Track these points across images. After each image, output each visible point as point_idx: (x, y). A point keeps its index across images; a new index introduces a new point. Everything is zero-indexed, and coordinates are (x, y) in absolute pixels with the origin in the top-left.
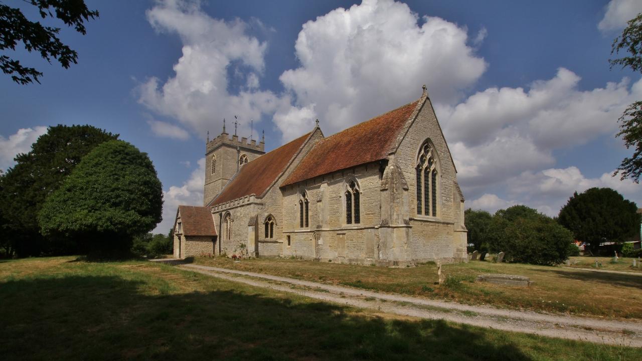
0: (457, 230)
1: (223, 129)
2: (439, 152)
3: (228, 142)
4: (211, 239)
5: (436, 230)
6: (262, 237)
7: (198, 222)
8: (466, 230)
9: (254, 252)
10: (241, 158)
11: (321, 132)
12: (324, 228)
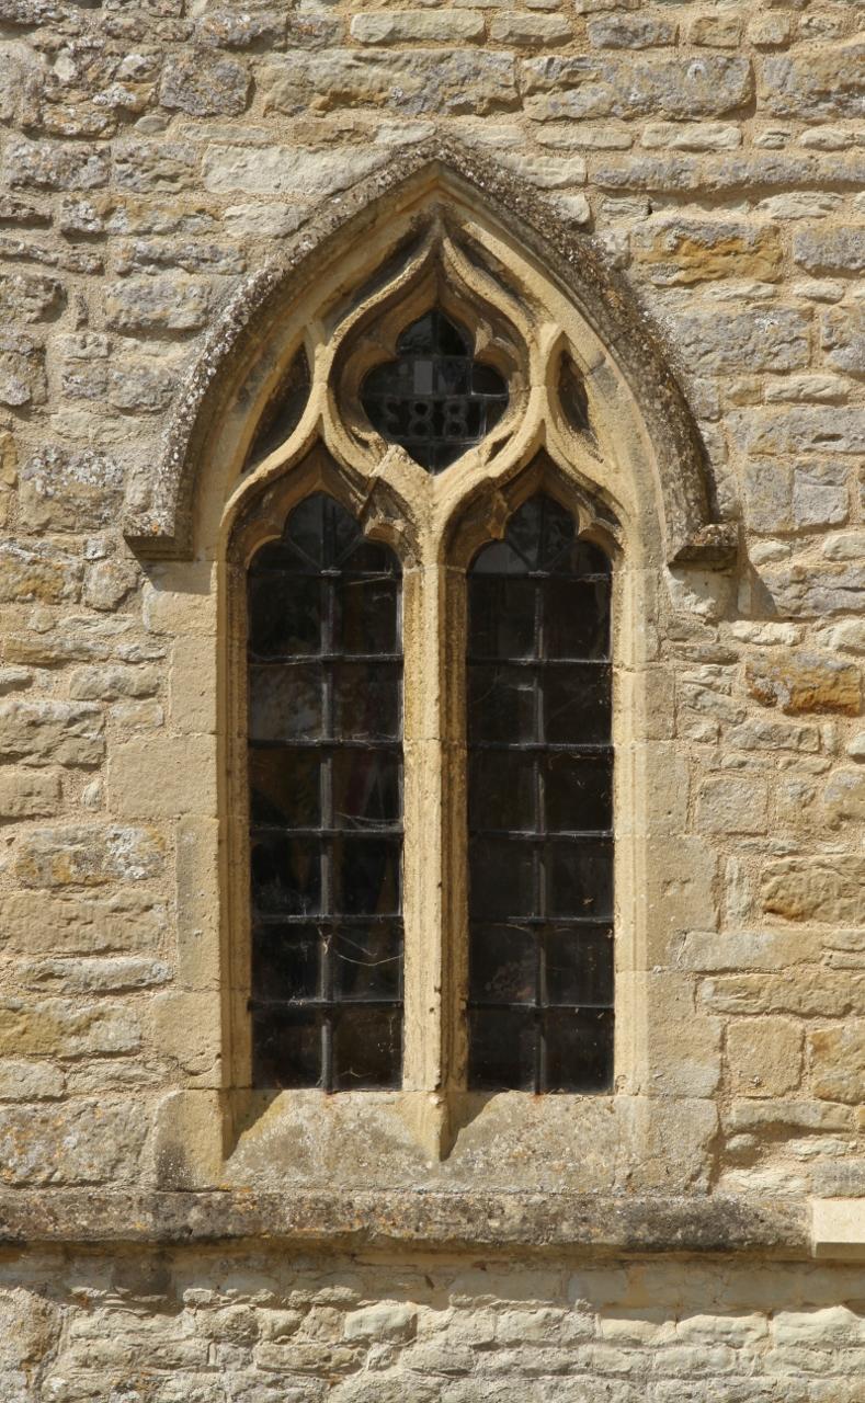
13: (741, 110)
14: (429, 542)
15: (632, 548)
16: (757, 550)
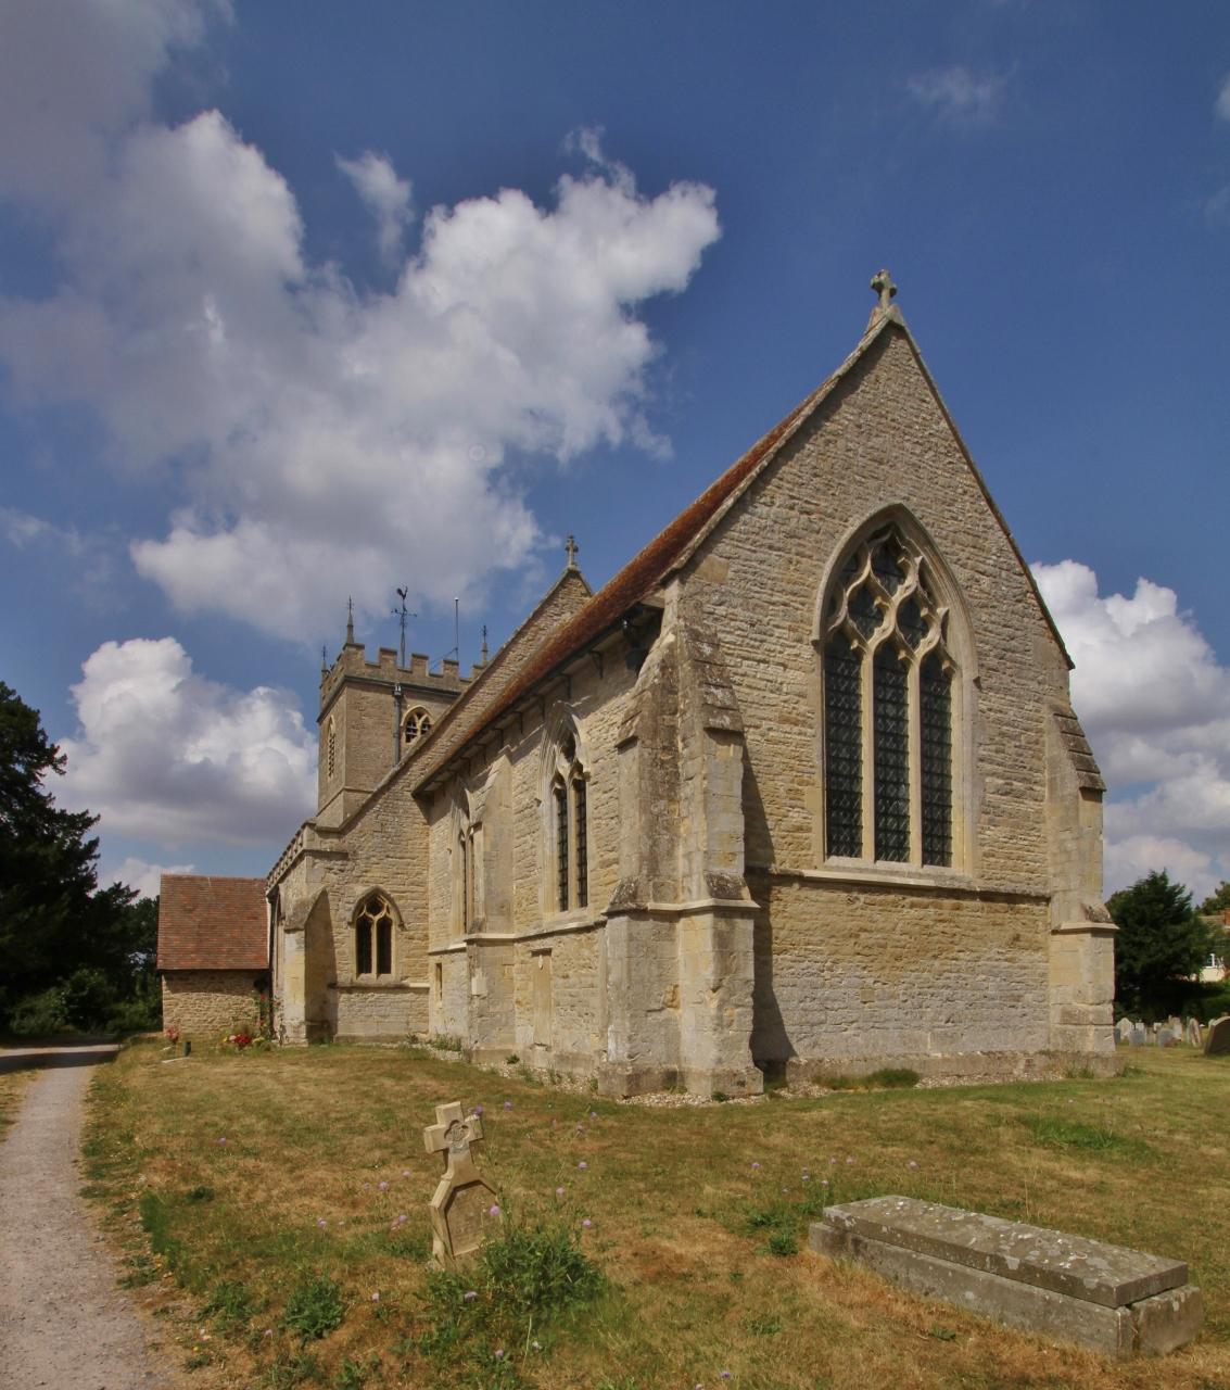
0: (1065, 926)
1: (346, 630)
2: (962, 575)
3: (366, 673)
4: (252, 982)
5: (940, 927)
6: (346, 969)
7: (213, 927)
8: (1113, 926)
9: (301, 1023)
10: (410, 721)
11: (584, 585)
12: (492, 930)
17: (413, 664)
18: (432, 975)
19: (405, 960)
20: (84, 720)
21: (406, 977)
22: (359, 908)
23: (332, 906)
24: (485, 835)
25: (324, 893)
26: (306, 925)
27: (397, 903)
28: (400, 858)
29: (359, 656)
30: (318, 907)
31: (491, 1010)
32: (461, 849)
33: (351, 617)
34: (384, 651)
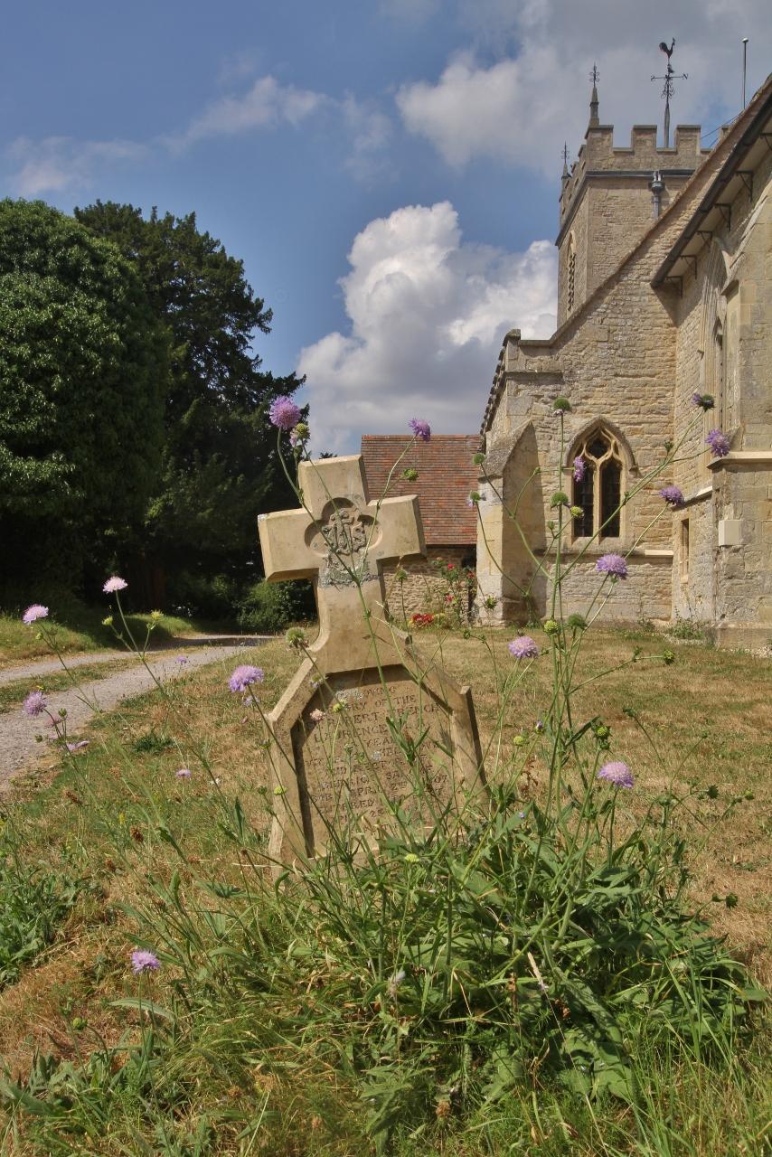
3: (613, 164)
12: (753, 445)
13: (639, 413)
14: (598, 468)
15: (624, 468)
16: (640, 469)
17: (678, 142)
18: (676, 540)
19: (638, 518)
20: (352, 316)
21: (641, 542)
22: (576, 450)
23: (541, 445)
24: (742, 300)
25: (530, 429)
26: (504, 470)
27: (630, 439)
28: (633, 376)
29: (606, 143)
30: (523, 447)
31: (748, 568)
32: (717, 348)
33: (595, 91)
34: (639, 130)
